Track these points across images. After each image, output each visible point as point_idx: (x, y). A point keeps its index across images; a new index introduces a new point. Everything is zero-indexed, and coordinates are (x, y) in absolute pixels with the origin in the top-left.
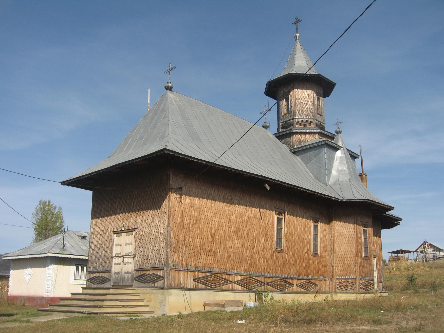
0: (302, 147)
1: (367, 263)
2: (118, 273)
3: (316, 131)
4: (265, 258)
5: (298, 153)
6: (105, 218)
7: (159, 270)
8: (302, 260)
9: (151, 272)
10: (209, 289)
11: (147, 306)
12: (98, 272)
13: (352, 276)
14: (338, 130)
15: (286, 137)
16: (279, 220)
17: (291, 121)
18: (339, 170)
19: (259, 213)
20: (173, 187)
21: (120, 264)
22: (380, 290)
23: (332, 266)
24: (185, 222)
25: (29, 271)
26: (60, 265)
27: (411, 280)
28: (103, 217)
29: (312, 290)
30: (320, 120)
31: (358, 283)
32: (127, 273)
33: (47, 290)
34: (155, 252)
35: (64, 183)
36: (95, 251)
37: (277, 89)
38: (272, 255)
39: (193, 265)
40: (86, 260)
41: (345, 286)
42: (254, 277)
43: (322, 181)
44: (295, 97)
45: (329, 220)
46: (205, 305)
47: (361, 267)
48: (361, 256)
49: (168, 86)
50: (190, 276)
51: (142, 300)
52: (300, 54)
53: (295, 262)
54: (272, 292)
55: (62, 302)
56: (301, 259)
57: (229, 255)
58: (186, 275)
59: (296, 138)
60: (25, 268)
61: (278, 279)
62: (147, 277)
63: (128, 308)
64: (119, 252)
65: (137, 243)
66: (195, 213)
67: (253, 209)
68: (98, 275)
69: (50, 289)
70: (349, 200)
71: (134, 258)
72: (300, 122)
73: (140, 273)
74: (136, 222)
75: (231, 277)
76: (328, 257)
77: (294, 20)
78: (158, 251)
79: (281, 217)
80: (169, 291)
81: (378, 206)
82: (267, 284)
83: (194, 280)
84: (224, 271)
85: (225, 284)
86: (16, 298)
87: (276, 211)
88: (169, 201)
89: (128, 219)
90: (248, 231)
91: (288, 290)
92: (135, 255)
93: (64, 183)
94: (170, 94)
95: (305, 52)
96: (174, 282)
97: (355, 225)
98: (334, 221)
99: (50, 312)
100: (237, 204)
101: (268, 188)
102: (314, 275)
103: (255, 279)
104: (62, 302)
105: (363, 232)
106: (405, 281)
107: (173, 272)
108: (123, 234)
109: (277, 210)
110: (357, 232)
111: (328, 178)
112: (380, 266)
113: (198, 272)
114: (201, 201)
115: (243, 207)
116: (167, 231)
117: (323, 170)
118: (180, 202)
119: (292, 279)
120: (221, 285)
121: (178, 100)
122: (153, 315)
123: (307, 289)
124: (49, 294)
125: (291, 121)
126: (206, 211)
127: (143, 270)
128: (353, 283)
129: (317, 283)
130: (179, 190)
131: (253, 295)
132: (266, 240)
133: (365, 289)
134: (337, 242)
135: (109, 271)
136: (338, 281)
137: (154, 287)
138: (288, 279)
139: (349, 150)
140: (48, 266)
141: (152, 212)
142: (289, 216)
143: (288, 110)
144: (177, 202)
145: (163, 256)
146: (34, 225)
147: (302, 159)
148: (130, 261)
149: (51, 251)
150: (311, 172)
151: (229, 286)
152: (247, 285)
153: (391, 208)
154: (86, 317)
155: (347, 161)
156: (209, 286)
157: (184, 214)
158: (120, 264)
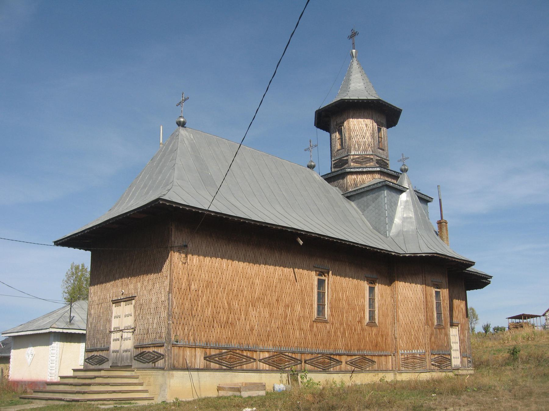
0: (357, 190)
1: (441, 333)
2: (117, 352)
3: (375, 169)
4: (301, 329)
5: (353, 198)
6: (104, 285)
7: (159, 346)
8: (353, 331)
9: (151, 350)
10: (225, 370)
11: (146, 391)
12: (96, 350)
13: (421, 351)
14: (403, 167)
15: (339, 179)
16: (321, 283)
17: (345, 158)
18: (404, 218)
19: (292, 274)
20: (176, 244)
21: (118, 340)
22: (465, 367)
23: (395, 338)
24: (193, 287)
25: (31, 350)
26: (67, 342)
27: (513, 354)
28: (102, 283)
29: (368, 369)
30: (382, 156)
31: (429, 358)
32: (126, 351)
33: (51, 373)
34: (157, 324)
35: (58, 243)
36: (93, 325)
37: (330, 118)
38: (311, 326)
39: (204, 340)
40: (84, 335)
41: (412, 362)
42: (287, 354)
43: (382, 232)
44: (349, 129)
45: (389, 280)
46: (219, 389)
47: (433, 339)
48: (433, 324)
49: (180, 122)
50: (199, 353)
51: (141, 384)
52: (357, 75)
53: (344, 333)
54: (310, 371)
55: (49, 388)
56: (351, 329)
57: (252, 327)
58: (193, 353)
59: (350, 179)
60: (27, 347)
61: (320, 355)
62: (147, 356)
63: (120, 394)
64: (117, 326)
65: (137, 314)
66: (204, 276)
67: (285, 269)
68: (95, 353)
69: (54, 371)
70: (413, 255)
71: (133, 332)
72: (356, 158)
73: (139, 351)
74: (136, 289)
75: (255, 354)
76: (390, 327)
77: (350, 34)
78: (158, 324)
79: (323, 278)
80: (171, 372)
81: (452, 261)
82: (305, 362)
83: (205, 358)
84: (245, 347)
85: (247, 362)
86: (16, 383)
87: (316, 271)
88: (171, 262)
89: (127, 285)
90: (278, 297)
91: (333, 369)
92: (134, 329)
93: (58, 243)
94: (182, 131)
95: (364, 73)
96: (178, 361)
97: (424, 286)
98: (396, 282)
99: (31, 400)
100: (263, 264)
101: (301, 243)
102: (370, 350)
103: (289, 356)
104: (49, 388)
105: (434, 294)
106: (506, 355)
107: (176, 350)
108: (122, 303)
109: (317, 269)
110: (426, 294)
111: (389, 227)
112: (464, 336)
113: (210, 348)
114: (214, 262)
115: (271, 266)
116: (169, 299)
117: (382, 218)
118: (185, 263)
119: (340, 355)
120: (241, 364)
121: (192, 137)
122: (151, 402)
123: (361, 368)
124: (53, 378)
125: (345, 158)
126: (220, 273)
127: (143, 348)
128: (422, 359)
129: (375, 359)
130: (184, 249)
131: (285, 375)
132: (303, 307)
133: (439, 366)
134: (401, 308)
135: (108, 349)
136: (403, 357)
137: (154, 368)
138: (334, 355)
139: (418, 192)
140: (51, 344)
141: (152, 276)
142: (335, 277)
143: (342, 144)
144: (181, 263)
145: (164, 330)
146: (64, 294)
147: (357, 205)
148: (129, 337)
149: (54, 326)
150: (368, 221)
151: (254, 365)
152: (277, 363)
153: (471, 264)
154: (64, 406)
155: (414, 206)
156: (225, 366)
157: (191, 278)
158: (118, 340)
